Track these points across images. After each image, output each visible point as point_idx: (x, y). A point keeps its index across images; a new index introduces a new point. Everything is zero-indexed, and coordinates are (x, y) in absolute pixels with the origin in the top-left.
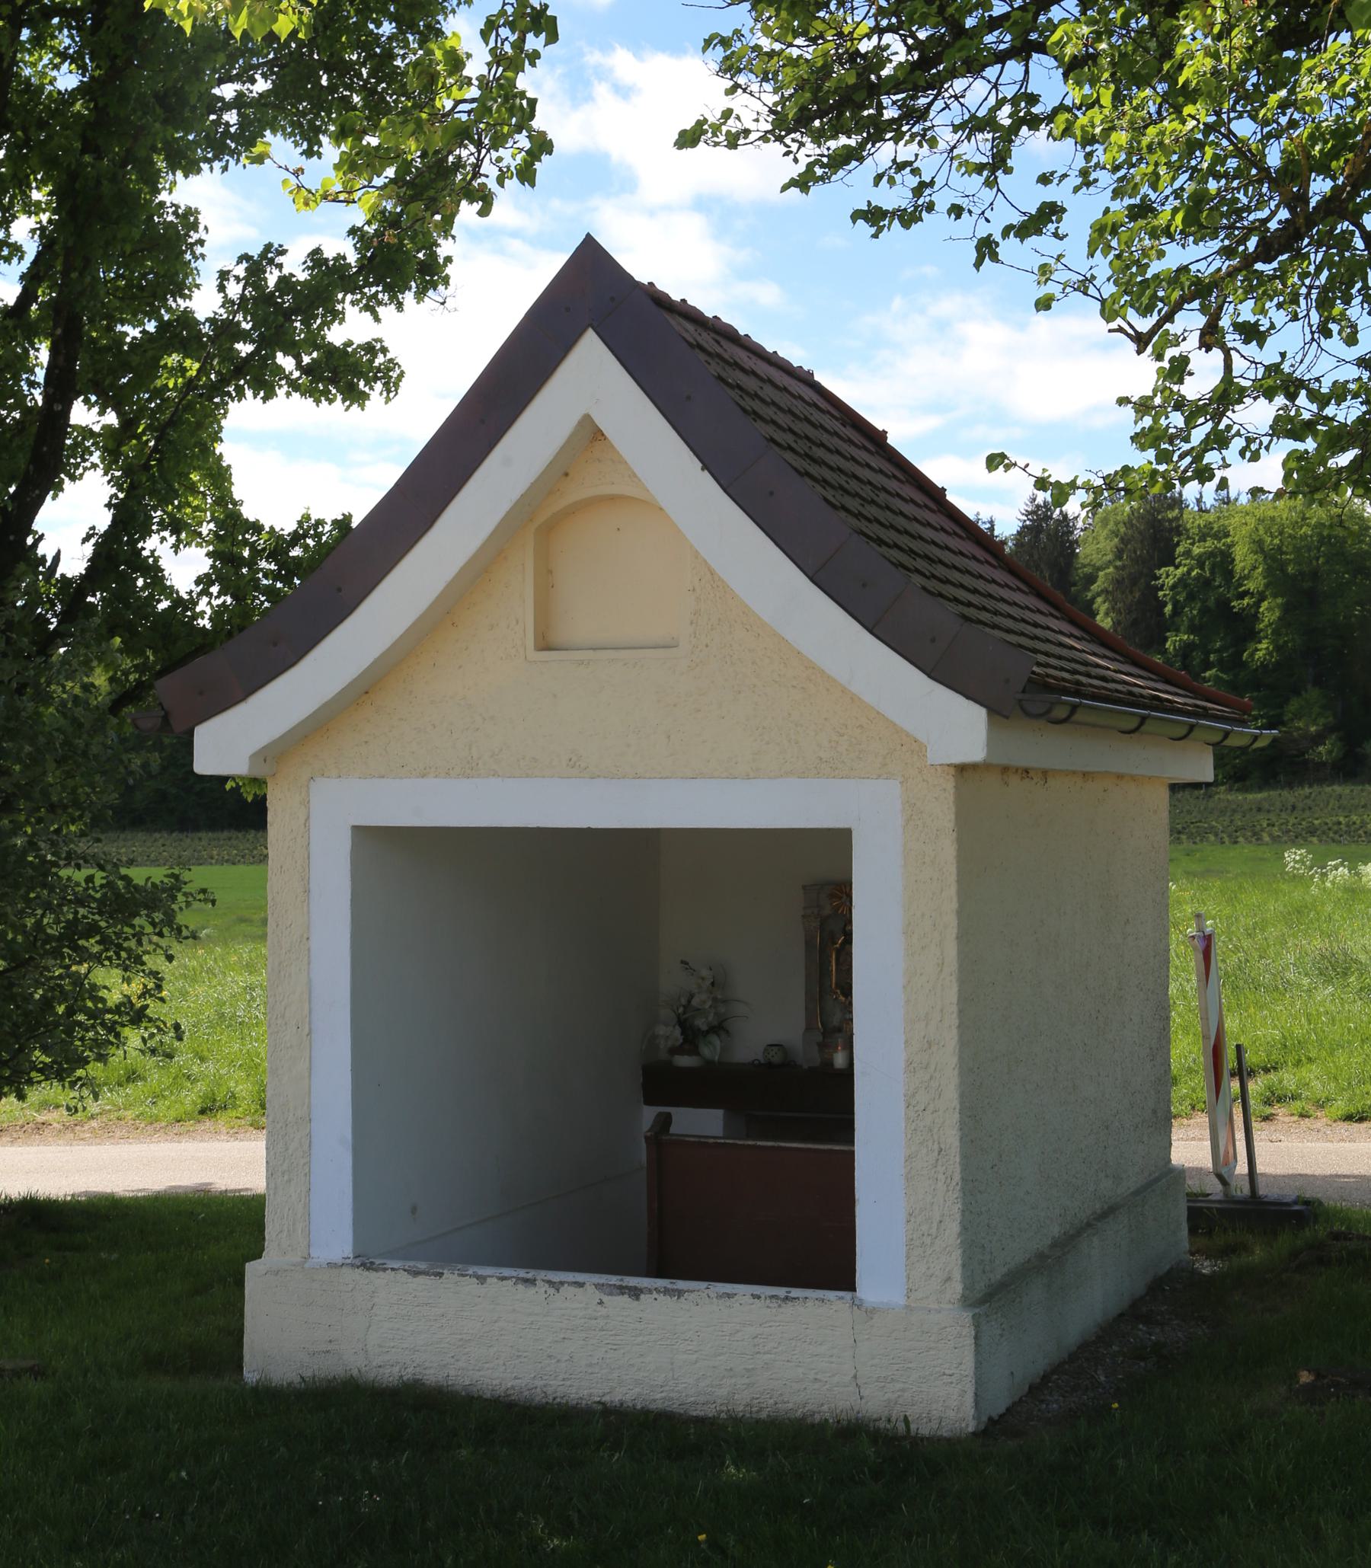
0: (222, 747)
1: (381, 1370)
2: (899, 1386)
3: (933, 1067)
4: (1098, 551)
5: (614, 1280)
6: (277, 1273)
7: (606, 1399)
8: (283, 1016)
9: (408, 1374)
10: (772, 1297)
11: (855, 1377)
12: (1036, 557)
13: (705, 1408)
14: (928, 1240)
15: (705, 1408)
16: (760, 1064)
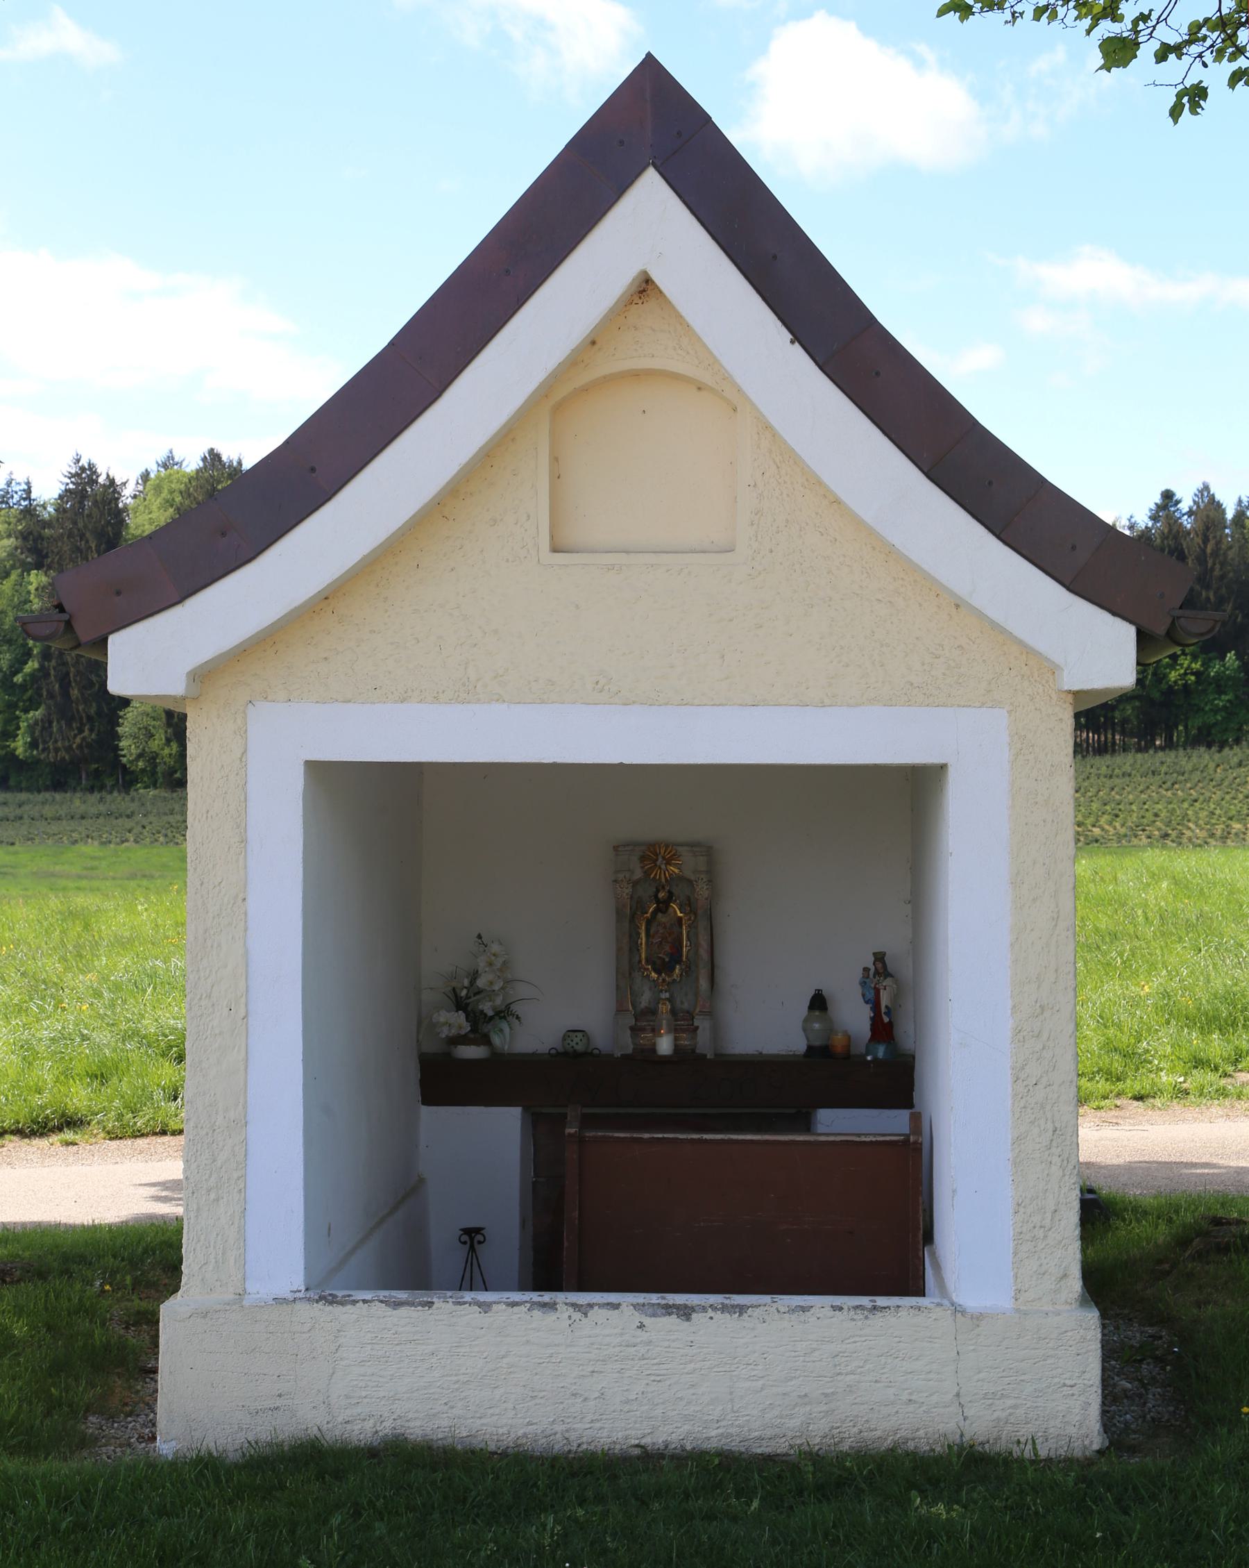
0: (145, 661)
1: (349, 1427)
2: (1010, 1402)
3: (1045, 1036)
4: (151, 521)
5: (654, 1298)
6: (205, 1315)
7: (647, 1441)
8: (209, 996)
9: (387, 1428)
10: (856, 1308)
11: (958, 1395)
12: (81, 525)
13: (773, 1443)
14: (1041, 1233)
15: (773, 1443)
16: (558, 1054)
